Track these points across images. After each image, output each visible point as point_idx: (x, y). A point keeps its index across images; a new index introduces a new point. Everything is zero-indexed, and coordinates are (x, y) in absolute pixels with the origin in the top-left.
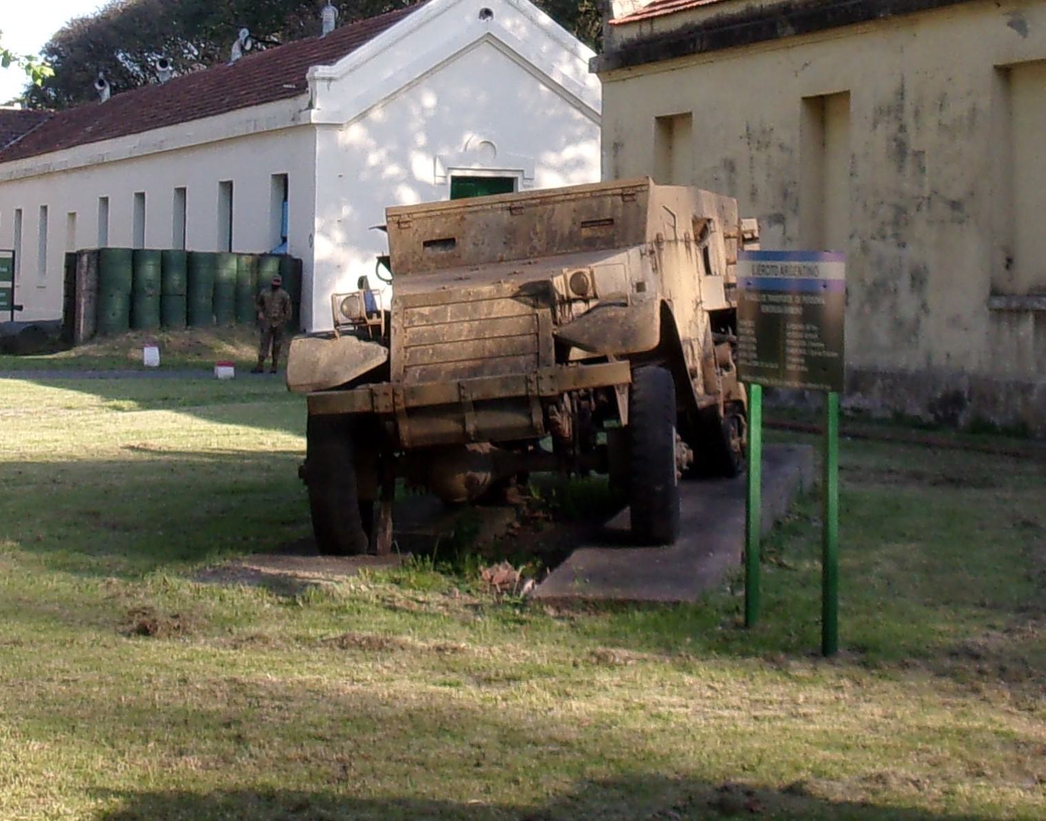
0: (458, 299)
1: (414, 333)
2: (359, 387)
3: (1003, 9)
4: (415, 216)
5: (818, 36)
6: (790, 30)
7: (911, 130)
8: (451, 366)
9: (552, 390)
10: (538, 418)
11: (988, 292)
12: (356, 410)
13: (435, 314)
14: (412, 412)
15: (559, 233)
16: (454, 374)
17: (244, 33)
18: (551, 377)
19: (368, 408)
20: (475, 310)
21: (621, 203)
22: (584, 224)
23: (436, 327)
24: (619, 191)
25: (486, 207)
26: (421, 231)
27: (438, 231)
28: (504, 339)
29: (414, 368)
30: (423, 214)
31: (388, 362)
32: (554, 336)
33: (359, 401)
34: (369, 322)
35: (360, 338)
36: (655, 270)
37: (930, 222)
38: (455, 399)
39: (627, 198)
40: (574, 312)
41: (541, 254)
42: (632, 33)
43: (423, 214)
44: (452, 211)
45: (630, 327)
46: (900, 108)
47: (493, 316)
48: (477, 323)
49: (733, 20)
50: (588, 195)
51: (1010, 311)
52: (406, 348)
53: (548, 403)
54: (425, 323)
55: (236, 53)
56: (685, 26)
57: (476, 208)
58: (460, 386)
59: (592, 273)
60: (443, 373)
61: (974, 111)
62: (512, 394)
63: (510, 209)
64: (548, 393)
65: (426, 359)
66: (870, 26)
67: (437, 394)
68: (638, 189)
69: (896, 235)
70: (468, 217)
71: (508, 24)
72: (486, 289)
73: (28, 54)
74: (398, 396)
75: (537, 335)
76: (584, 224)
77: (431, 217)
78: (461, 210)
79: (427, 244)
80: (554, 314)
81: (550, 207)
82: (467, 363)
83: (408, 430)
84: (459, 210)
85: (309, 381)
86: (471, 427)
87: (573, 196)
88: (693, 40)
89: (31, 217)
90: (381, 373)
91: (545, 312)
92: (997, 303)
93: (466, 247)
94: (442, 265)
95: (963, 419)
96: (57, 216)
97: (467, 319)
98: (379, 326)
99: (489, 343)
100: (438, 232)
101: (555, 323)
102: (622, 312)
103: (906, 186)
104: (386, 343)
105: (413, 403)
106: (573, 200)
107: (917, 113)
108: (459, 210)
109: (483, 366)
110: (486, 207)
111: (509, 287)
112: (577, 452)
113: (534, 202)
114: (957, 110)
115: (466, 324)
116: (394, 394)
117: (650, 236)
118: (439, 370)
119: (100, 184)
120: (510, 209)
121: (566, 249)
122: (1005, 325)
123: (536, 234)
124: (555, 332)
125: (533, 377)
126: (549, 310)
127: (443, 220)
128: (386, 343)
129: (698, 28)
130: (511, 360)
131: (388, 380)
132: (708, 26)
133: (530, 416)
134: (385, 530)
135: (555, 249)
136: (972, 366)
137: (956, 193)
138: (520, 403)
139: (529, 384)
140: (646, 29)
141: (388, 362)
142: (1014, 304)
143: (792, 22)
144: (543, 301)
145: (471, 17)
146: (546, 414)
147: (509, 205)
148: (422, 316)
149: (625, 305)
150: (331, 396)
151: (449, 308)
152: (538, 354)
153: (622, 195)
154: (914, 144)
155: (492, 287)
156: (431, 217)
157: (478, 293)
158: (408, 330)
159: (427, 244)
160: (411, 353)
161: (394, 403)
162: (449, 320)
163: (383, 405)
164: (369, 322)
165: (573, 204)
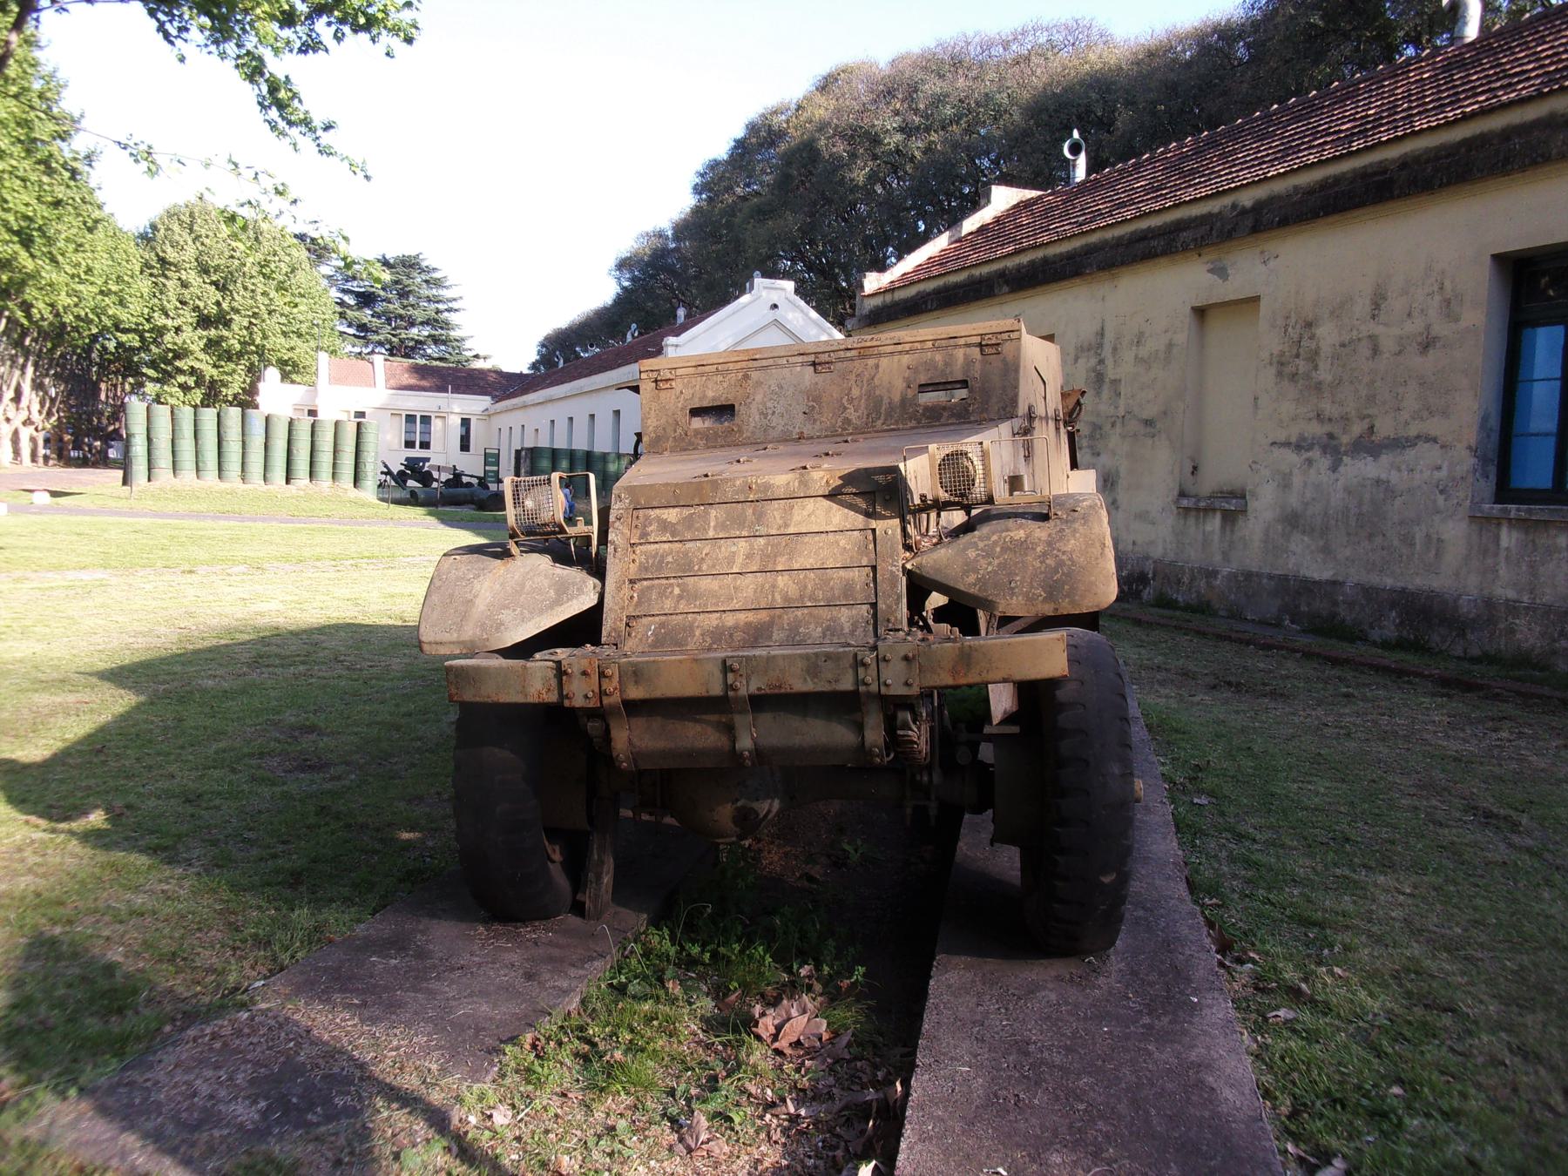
0: (729, 497)
1: (647, 555)
2: (537, 656)
3: (1205, 258)
4: (679, 372)
5: (1030, 292)
6: (1006, 289)
7: (1109, 362)
8: (712, 621)
9: (907, 684)
10: (875, 735)
11: (1176, 493)
12: (530, 700)
13: (688, 522)
14: (633, 708)
15: (886, 401)
16: (717, 635)
17: (634, 326)
18: (906, 658)
19: (552, 697)
20: (760, 517)
21: (979, 356)
22: (924, 388)
23: (689, 545)
24: (977, 340)
25: (780, 361)
26: (688, 393)
27: (710, 394)
28: (812, 575)
29: (645, 621)
30: (692, 370)
31: (597, 610)
32: (909, 574)
33: (535, 681)
34: (571, 531)
35: (556, 560)
36: (1027, 458)
37: (1123, 437)
38: (717, 690)
39: (986, 350)
40: (943, 522)
41: (859, 431)
42: (878, 301)
43: (692, 370)
44: (731, 366)
45: (1061, 564)
46: (1100, 346)
47: (791, 530)
48: (762, 541)
49: (957, 286)
50: (930, 344)
51: (1198, 510)
52: (632, 582)
53: (892, 706)
54: (668, 537)
55: (629, 338)
56: (918, 293)
57: (764, 363)
58: (726, 668)
59: (985, 456)
60: (697, 633)
61: (1170, 346)
62: (826, 688)
63: (814, 364)
64: (900, 690)
65: (668, 605)
66: (1078, 280)
67: (678, 682)
68: (1005, 336)
69: (1091, 447)
70: (754, 375)
71: (790, 316)
72: (781, 479)
73: (232, 176)
74: (610, 677)
75: (874, 568)
76: (924, 388)
77: (702, 374)
78: (744, 365)
79: (696, 412)
80: (904, 530)
81: (871, 362)
82: (742, 617)
83: (625, 738)
84: (739, 366)
85: (454, 637)
86: (745, 743)
87: (907, 347)
88: (925, 303)
89: (505, 432)
90: (583, 629)
91: (889, 527)
92: (1185, 503)
93: (749, 417)
94: (712, 442)
95: (1148, 594)
96: (529, 431)
97: (745, 533)
98: (588, 539)
99: (782, 581)
100: (713, 393)
101: (908, 547)
102: (1040, 531)
103: (1103, 408)
104: (597, 568)
105: (635, 693)
106: (907, 352)
107: (1115, 349)
108: (739, 366)
109: (771, 624)
110: (780, 361)
111: (825, 474)
112: (936, 778)
113: (849, 354)
114: (1153, 345)
115: (742, 543)
116: (602, 675)
117: (1022, 409)
118: (690, 629)
119: (551, 412)
120: (814, 364)
121: (897, 423)
122: (1191, 521)
123: (851, 401)
124: (909, 566)
125: (869, 658)
126: (897, 521)
127: (720, 378)
128: (597, 568)
129: (929, 294)
130: (825, 613)
131: (596, 642)
132: (937, 292)
133: (859, 728)
134: (599, 877)
135: (879, 422)
136: (1157, 552)
137: (1150, 412)
138: (843, 705)
139: (861, 670)
140: (888, 298)
141: (597, 610)
142: (1202, 504)
143: (1007, 282)
144: (886, 506)
145: (766, 309)
146: (891, 726)
147: (812, 358)
148: (664, 526)
149: (1044, 518)
150: (477, 669)
151: (713, 512)
152: (874, 605)
153: (980, 345)
154: (1111, 373)
155: (791, 476)
156: (702, 374)
157: (767, 486)
158: (638, 549)
159: (696, 412)
160: (642, 593)
161: (602, 693)
162: (711, 534)
163: (580, 693)
164: (571, 531)
165: (906, 359)
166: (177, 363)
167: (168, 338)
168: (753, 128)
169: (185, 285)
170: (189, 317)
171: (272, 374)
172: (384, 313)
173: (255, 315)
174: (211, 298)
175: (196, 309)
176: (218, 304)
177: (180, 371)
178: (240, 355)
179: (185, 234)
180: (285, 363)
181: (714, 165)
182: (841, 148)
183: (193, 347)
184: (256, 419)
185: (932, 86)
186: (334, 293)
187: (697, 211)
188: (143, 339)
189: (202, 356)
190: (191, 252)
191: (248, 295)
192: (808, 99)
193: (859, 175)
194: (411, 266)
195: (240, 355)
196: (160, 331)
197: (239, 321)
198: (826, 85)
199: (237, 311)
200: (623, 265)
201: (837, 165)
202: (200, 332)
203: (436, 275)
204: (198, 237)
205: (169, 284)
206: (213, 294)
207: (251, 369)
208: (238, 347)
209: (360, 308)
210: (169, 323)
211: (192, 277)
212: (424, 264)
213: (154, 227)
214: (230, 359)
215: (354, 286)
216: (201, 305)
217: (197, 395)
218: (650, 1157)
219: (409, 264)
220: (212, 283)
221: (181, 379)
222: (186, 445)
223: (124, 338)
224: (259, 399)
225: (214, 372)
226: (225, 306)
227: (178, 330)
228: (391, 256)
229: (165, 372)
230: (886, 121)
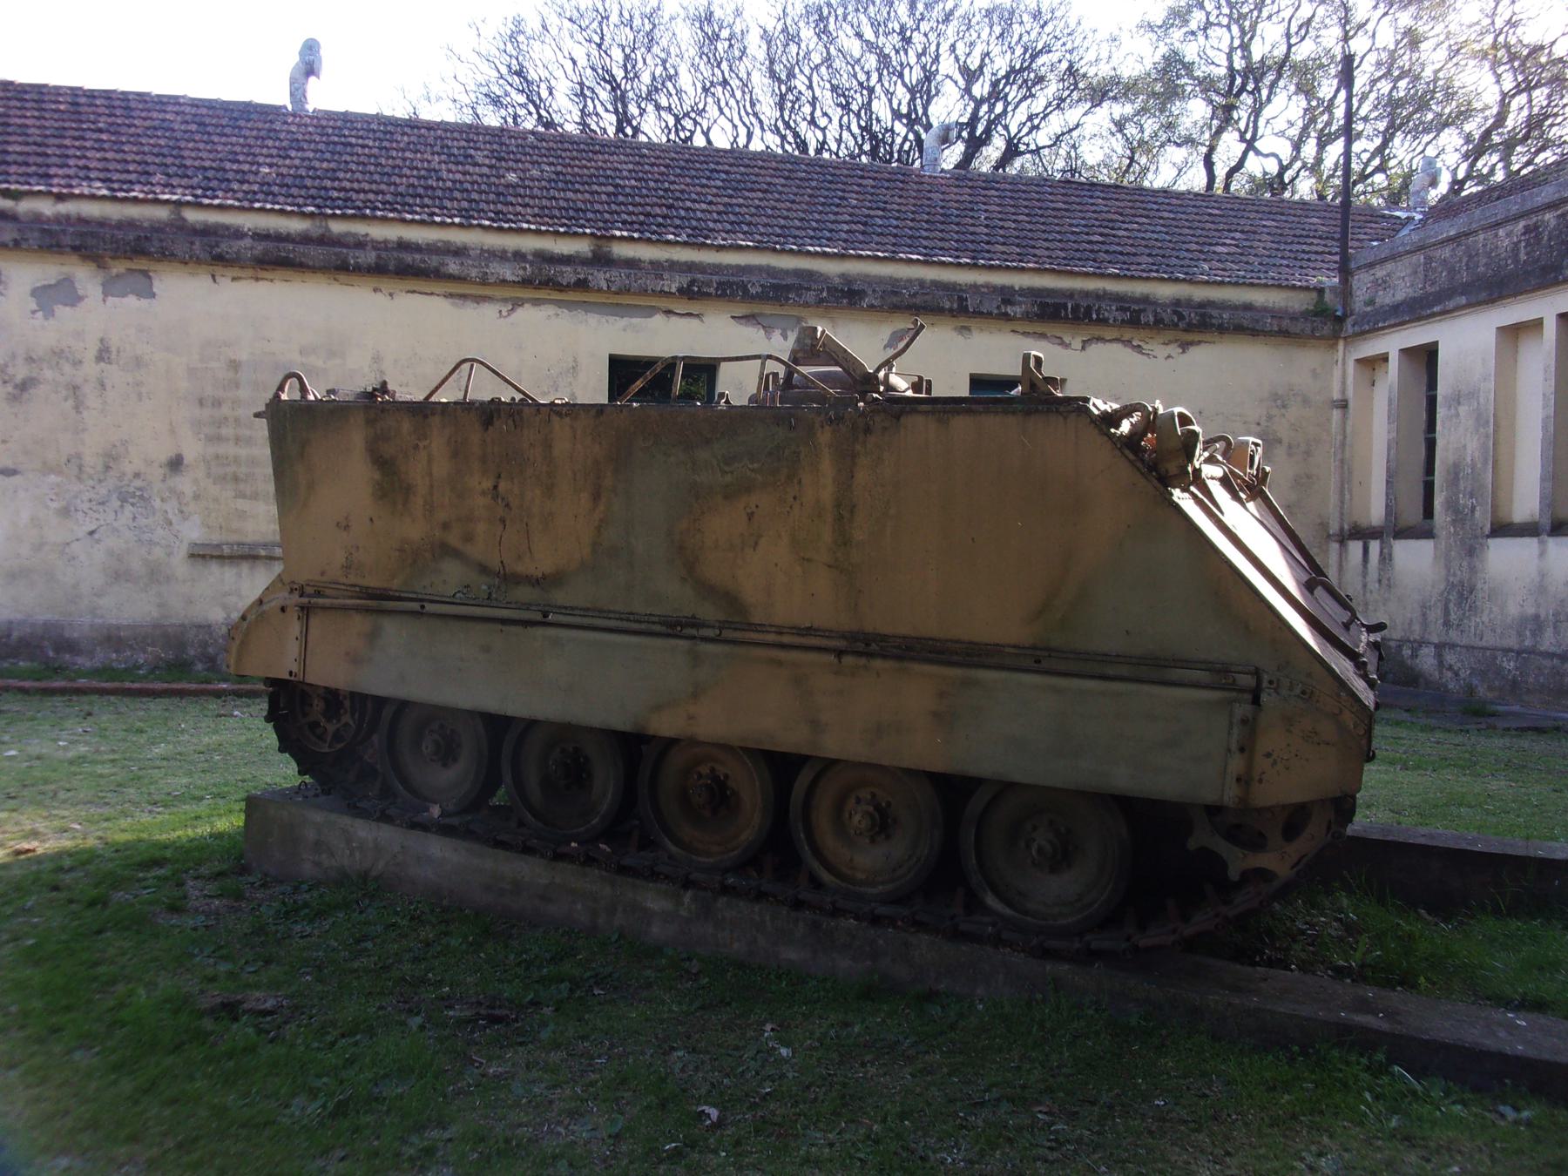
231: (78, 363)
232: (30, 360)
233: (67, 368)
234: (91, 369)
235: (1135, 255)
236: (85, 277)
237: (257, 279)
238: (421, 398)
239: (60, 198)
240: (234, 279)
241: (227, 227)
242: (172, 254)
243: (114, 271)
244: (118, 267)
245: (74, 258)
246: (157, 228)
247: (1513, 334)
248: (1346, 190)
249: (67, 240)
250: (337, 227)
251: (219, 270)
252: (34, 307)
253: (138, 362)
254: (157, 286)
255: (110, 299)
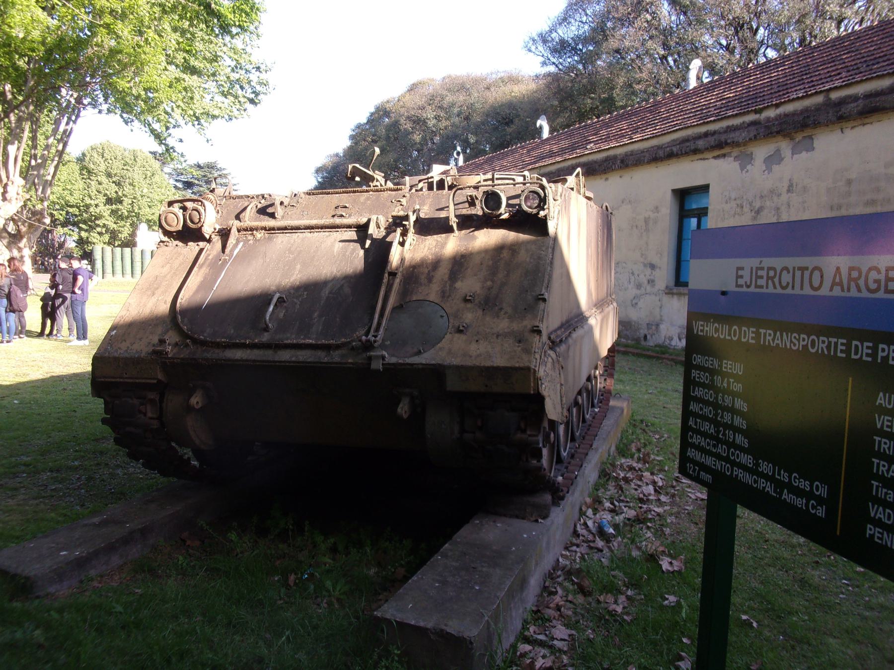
166: (97, 222)
167: (91, 209)
168: (378, 109)
169: (100, 184)
170: (102, 199)
171: (143, 227)
172: (198, 192)
173: (135, 198)
174: (112, 190)
175: (105, 195)
176: (116, 192)
177: (98, 226)
178: (127, 217)
179: (100, 159)
180: (150, 221)
181: (359, 126)
182: (408, 126)
183: (105, 214)
184: (137, 251)
185: (449, 98)
186: (172, 182)
187: (350, 148)
188: (80, 210)
189: (109, 218)
190: (103, 167)
191: (131, 187)
192: (403, 96)
193: (417, 138)
194: (212, 168)
195: (127, 217)
196: (88, 206)
197: (127, 201)
198: (413, 88)
199: (126, 196)
200: (318, 171)
201: (408, 133)
202: (107, 206)
203: (224, 172)
204: (106, 160)
205: (93, 183)
206: (114, 188)
207: (132, 225)
208: (126, 214)
209: (185, 189)
210: (92, 202)
211: (103, 179)
212: (219, 166)
213: (84, 155)
214: (122, 219)
215: (183, 178)
216: (108, 193)
217: (106, 238)
218: (317, 597)
219: (211, 167)
220: (113, 182)
221: (99, 229)
222: (118, 263)
223: (71, 210)
224: (137, 239)
225: (115, 226)
226: (120, 194)
227: (97, 206)
228: (202, 162)
229: (90, 226)
230: (429, 114)
231: (779, 195)
232: (762, 197)
233: (775, 198)
234: (785, 197)
235: (883, 38)
236: (785, 146)
237: (864, 125)
238: (164, 307)
239: (777, 106)
240: (852, 128)
241: (850, 97)
242: (819, 123)
243: (797, 140)
244: (799, 137)
245: (780, 138)
246: (818, 108)
247: (578, 175)
248: (91, 243)
249: (775, 129)
250: (820, 99)
251: (844, 124)
252: (764, 168)
253: (805, 189)
254: (816, 143)
255: (795, 156)
